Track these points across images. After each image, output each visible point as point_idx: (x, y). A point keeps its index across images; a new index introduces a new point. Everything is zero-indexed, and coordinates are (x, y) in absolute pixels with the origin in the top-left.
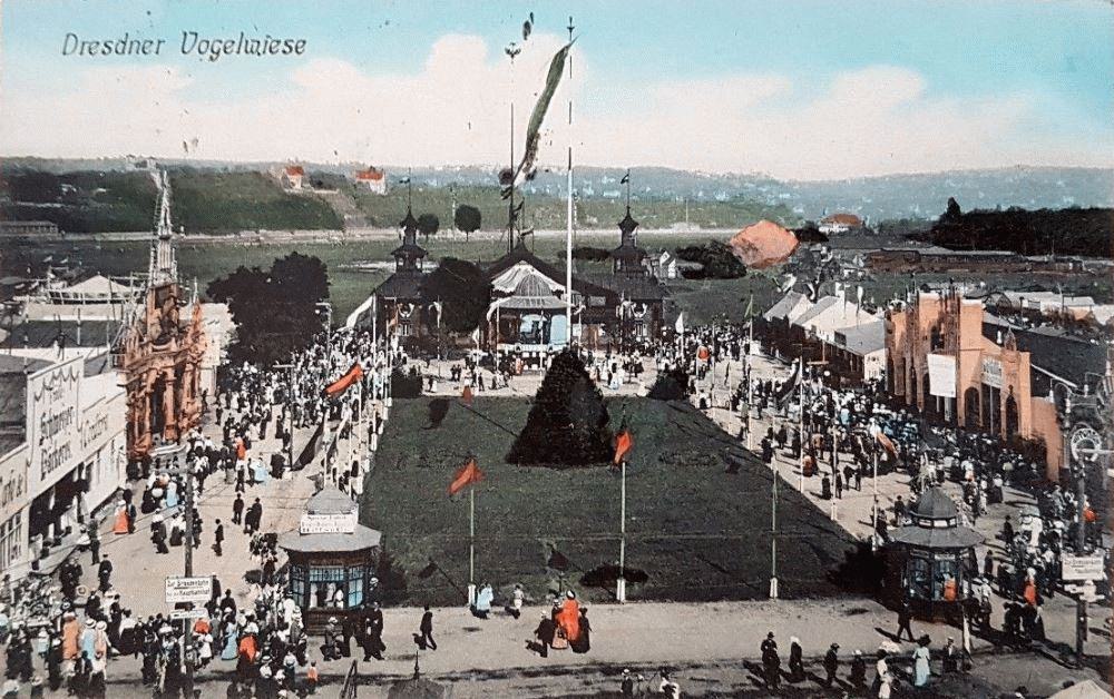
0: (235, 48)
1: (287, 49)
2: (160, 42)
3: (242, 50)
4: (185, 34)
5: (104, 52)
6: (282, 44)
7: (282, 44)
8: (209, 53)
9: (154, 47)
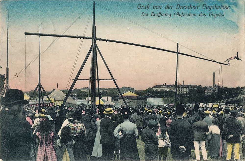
0: (219, 15)
1: (226, 8)
2: (198, 6)
3: (216, 8)
4: (203, 5)
5: (225, 8)
6: (225, 7)
7: (225, 7)
8: (214, 16)
9: (197, 8)
